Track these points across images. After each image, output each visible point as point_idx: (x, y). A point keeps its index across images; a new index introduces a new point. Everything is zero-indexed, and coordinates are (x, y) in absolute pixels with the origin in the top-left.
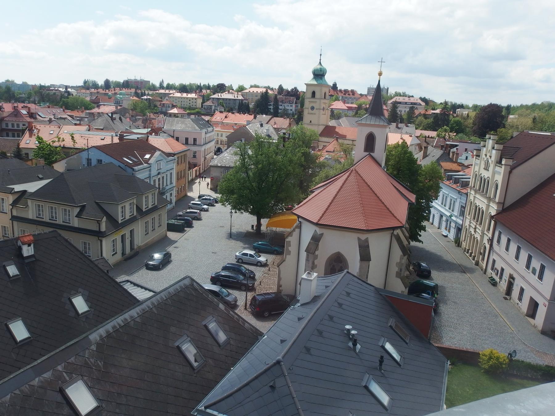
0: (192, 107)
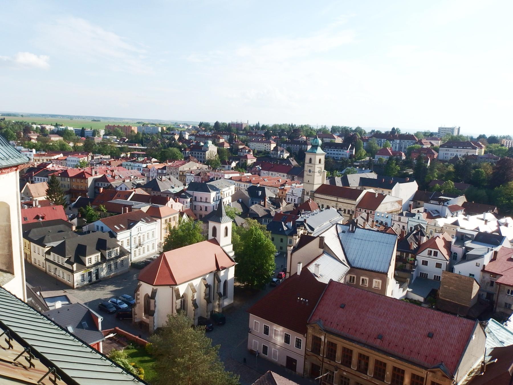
0: (267, 150)
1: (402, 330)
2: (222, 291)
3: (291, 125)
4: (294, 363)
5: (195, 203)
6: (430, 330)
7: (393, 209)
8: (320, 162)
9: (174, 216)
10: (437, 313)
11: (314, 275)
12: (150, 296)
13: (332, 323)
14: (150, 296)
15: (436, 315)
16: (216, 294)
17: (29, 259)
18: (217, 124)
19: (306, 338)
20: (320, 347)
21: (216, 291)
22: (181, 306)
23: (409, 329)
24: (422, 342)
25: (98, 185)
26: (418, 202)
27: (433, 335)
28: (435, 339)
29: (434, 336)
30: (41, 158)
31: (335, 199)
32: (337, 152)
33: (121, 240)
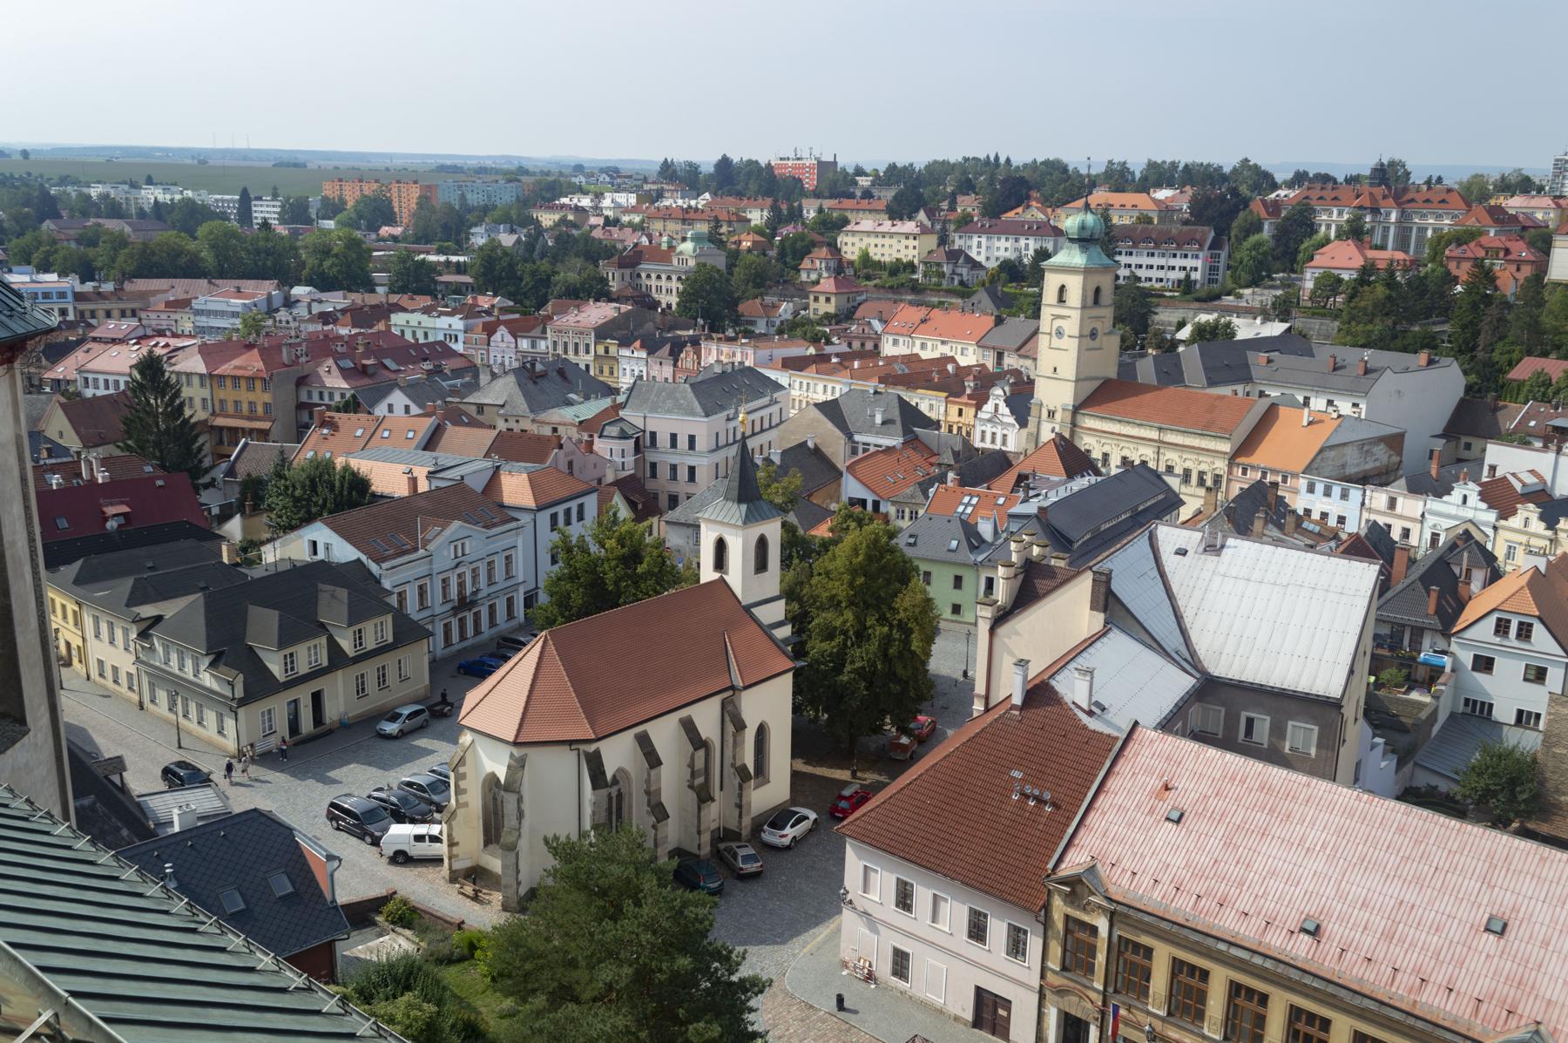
1: (1391, 904)
2: (749, 760)
3: (1002, 160)
4: (1002, 1012)
5: (651, 456)
6: (1496, 907)
7: (1367, 467)
8: (1061, 300)
9: (579, 501)
10: (1521, 847)
11: (1073, 707)
12: (502, 781)
13: (1137, 877)
14: (502, 781)
15: (1518, 855)
16: (728, 770)
17: (80, 661)
18: (724, 163)
19: (1045, 925)
20: (1094, 957)
21: (728, 760)
22: (610, 813)
23: (1418, 903)
24: (1465, 949)
25: (310, 396)
26: (1464, 439)
27: (1505, 926)
28: (1512, 939)
29: (1508, 929)
30: (100, 306)
31: (1154, 435)
32: (1162, 261)
33: (397, 590)
